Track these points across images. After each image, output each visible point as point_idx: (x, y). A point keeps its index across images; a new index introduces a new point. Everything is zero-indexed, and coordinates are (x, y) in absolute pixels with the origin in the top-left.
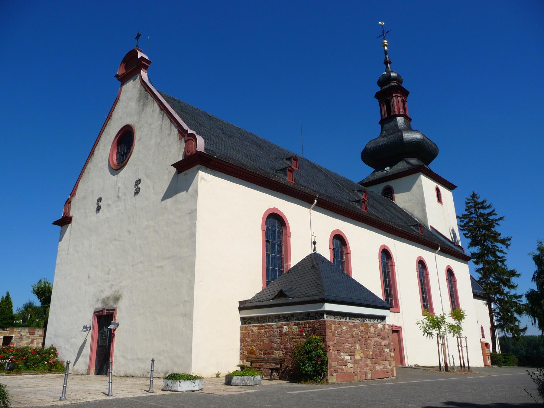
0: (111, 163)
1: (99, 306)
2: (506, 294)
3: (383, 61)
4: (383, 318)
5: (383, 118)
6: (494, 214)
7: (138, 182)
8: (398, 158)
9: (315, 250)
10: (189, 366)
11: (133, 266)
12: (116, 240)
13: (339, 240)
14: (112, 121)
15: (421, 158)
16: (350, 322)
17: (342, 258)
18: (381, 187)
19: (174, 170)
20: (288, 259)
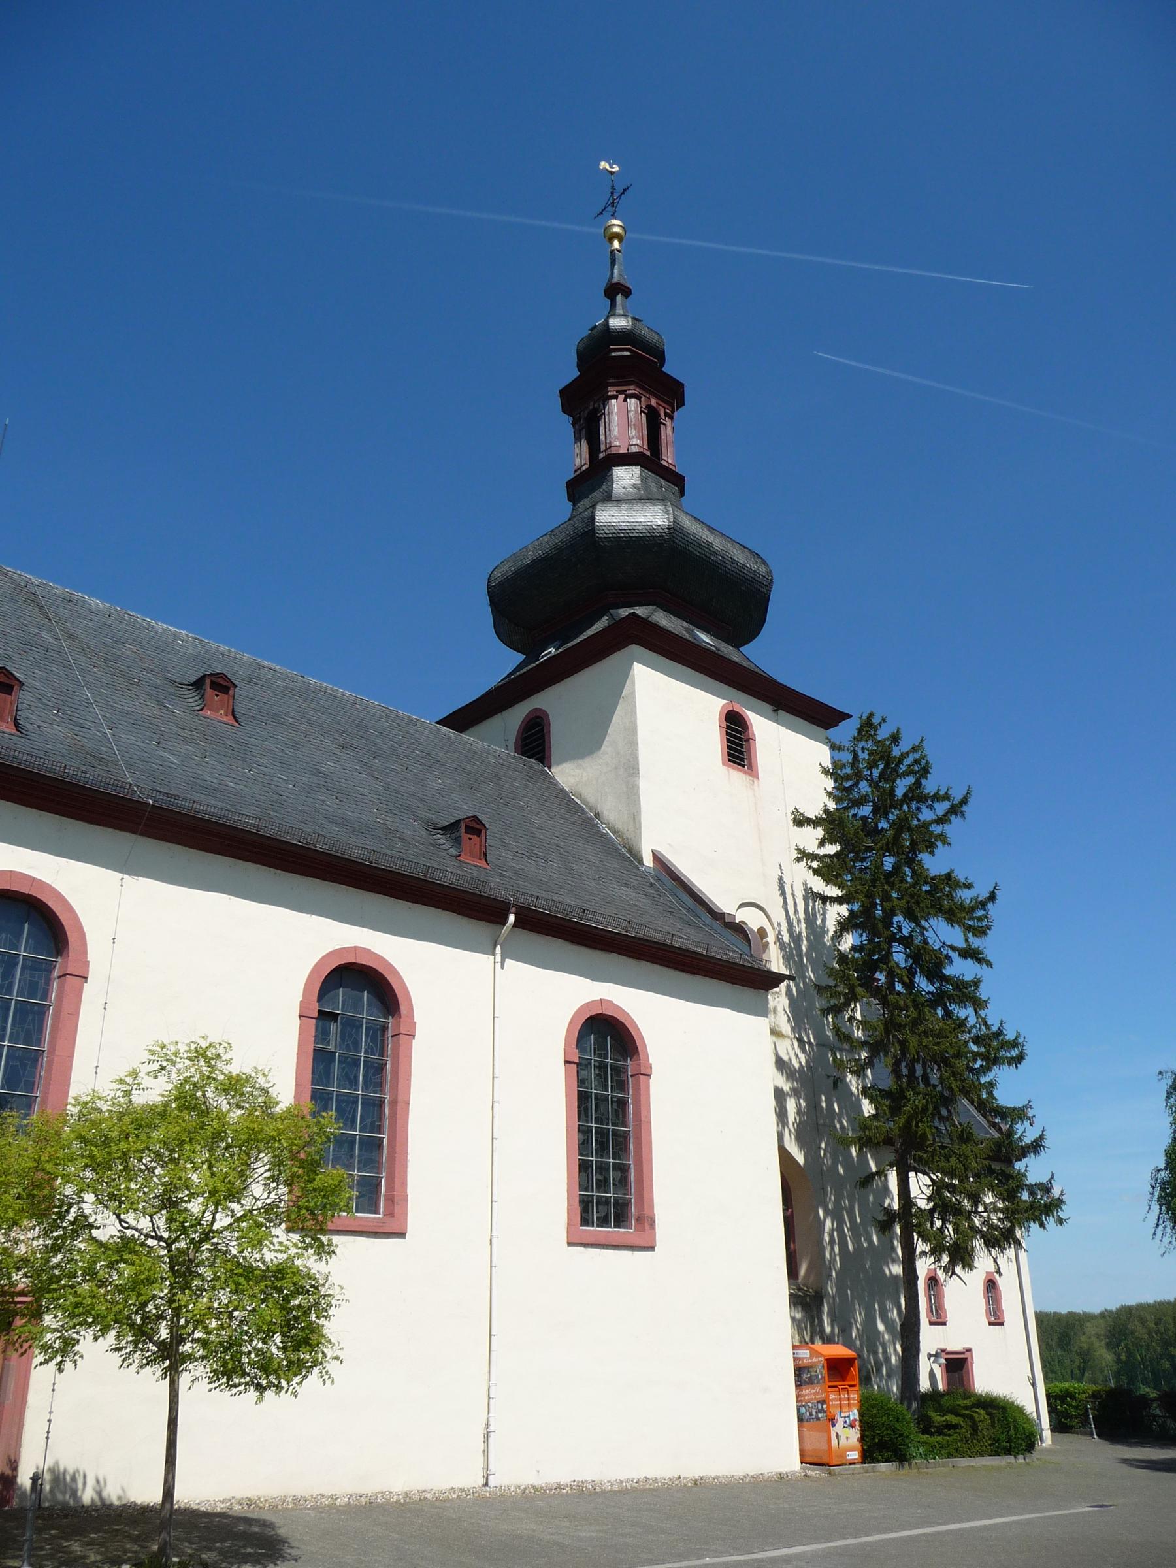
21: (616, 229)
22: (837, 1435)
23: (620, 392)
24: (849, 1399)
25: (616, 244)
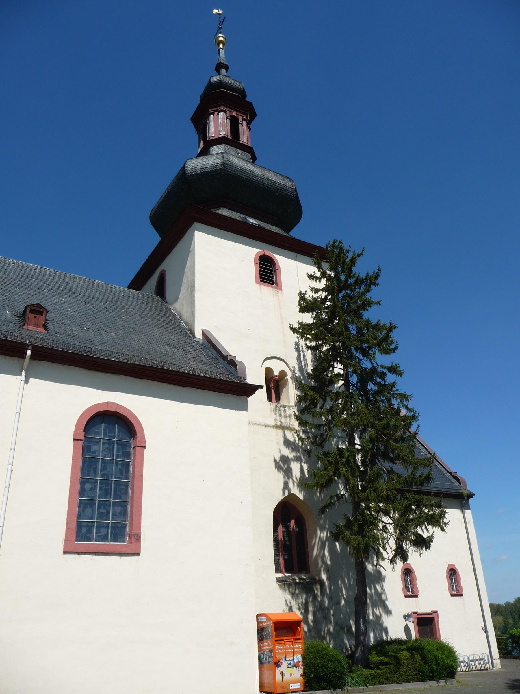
21: (221, 39)
22: (282, 673)
23: (215, 111)
24: (293, 648)
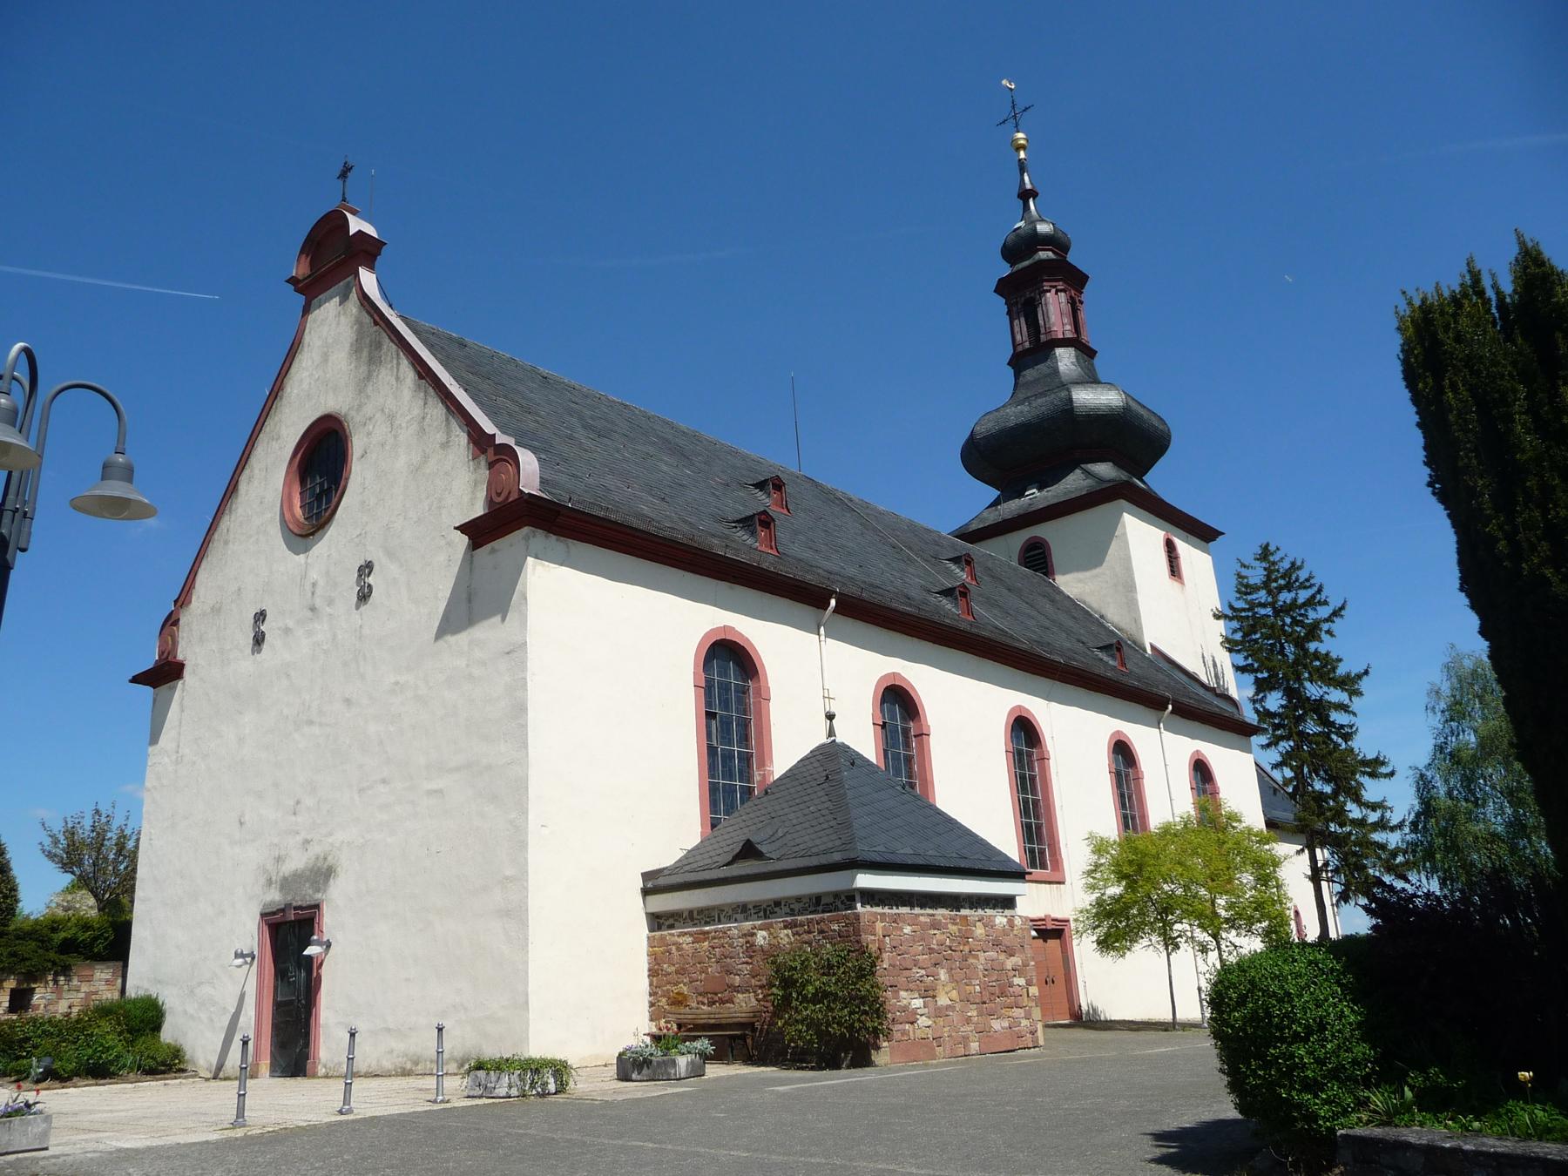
0: (287, 516)
1: (275, 897)
2: (1354, 822)
3: (1016, 191)
4: (1008, 902)
5: (1020, 349)
6: (1320, 603)
7: (366, 568)
8: (1065, 462)
9: (831, 733)
10: (525, 1039)
11: (361, 791)
12: (310, 723)
13: (898, 703)
14: (284, 401)
15: (1125, 452)
16: (923, 914)
17: (907, 745)
18: (1019, 539)
19: (462, 540)
20: (765, 757)
25: (1022, 155)
